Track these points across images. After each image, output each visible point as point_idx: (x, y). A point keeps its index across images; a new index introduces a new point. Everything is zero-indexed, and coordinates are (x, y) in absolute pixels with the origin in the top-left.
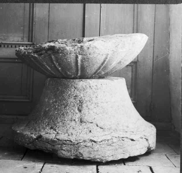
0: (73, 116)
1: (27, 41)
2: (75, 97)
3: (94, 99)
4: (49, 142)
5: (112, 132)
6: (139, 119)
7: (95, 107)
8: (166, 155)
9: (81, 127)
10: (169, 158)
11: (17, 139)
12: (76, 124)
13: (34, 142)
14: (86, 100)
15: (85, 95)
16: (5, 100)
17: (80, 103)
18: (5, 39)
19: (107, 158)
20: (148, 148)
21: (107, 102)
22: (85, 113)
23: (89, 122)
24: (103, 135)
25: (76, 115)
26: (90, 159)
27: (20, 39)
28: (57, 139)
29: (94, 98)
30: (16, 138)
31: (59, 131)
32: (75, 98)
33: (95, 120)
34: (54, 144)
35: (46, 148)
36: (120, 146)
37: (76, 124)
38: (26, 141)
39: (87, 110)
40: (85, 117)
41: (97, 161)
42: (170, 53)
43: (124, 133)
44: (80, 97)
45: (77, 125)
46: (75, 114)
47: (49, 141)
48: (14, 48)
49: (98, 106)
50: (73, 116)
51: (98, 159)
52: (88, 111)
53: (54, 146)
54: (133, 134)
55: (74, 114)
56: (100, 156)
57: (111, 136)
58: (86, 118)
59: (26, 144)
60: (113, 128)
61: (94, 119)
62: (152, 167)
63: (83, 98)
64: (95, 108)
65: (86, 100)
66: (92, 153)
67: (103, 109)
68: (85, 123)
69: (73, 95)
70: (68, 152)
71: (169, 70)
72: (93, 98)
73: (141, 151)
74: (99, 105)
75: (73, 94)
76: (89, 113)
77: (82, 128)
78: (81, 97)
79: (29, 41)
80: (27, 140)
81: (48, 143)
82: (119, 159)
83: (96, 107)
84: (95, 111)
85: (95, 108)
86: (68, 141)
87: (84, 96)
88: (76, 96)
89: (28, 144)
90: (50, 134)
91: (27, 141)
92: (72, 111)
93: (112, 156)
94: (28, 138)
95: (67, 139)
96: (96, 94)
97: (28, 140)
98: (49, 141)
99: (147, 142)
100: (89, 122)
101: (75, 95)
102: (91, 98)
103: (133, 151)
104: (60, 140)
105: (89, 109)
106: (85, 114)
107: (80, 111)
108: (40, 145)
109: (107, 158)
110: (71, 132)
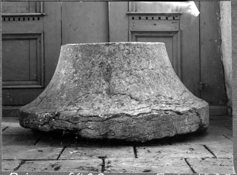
0: (99, 87)
1: (34, 11)
2: (100, 64)
3: (126, 66)
4: (70, 120)
5: (151, 105)
6: (185, 91)
7: (128, 75)
8: (223, 135)
9: (110, 100)
10: (228, 137)
11: (27, 122)
12: (103, 97)
13: (50, 122)
14: (115, 66)
15: (113, 62)
16: (9, 87)
17: (107, 72)
18: (5, 11)
19: (148, 136)
20: (199, 125)
21: (142, 70)
22: (114, 83)
23: (120, 94)
24: (138, 70)
25: (103, 87)
26: (124, 138)
27: (24, 9)
28: (79, 115)
29: (125, 65)
30: (26, 121)
31: (82, 106)
32: (100, 65)
33: (129, 91)
34: (76, 122)
35: (66, 127)
36: (164, 121)
37: (103, 97)
38: (40, 122)
39: (117, 80)
40: (115, 88)
41: (134, 141)
42: (221, 18)
43: (168, 106)
44: (107, 64)
45: (104, 99)
46: (102, 85)
47: (69, 119)
48: (17, 21)
49: (131, 74)
50: (99, 87)
51: (136, 137)
52: (119, 81)
53: (76, 124)
54: (179, 107)
55: (100, 85)
56: (137, 134)
57: (150, 109)
58: (116, 88)
59: (40, 126)
60: (153, 100)
61: (128, 89)
62: (207, 146)
63: (111, 65)
64: (128, 76)
65: (115, 66)
66: (127, 130)
67: (138, 77)
68: (115, 95)
69: (98, 63)
70: (96, 131)
71: (221, 40)
72: (124, 64)
73: (190, 127)
74: (132, 73)
75: (98, 61)
76: (120, 83)
77: (112, 102)
78: (109, 64)
79: (36, 12)
80: (40, 120)
81: (68, 121)
82: (163, 137)
83: (129, 76)
84: (127, 80)
85: (128, 76)
86: (94, 116)
87: (112, 63)
88: (102, 63)
89: (42, 125)
90: (70, 110)
91: (40, 122)
92: (98, 82)
93: (154, 133)
94: (41, 118)
95: (92, 114)
96: (128, 60)
97: (42, 121)
98: (69, 119)
99: (198, 117)
100: (120, 94)
101: (100, 62)
102: (121, 64)
103: (181, 127)
104: (84, 117)
105: (119, 78)
106: (115, 84)
107: (108, 81)
108: (57, 124)
109: (148, 136)
110: (98, 107)
